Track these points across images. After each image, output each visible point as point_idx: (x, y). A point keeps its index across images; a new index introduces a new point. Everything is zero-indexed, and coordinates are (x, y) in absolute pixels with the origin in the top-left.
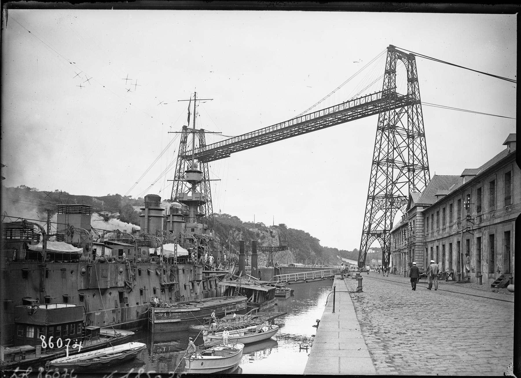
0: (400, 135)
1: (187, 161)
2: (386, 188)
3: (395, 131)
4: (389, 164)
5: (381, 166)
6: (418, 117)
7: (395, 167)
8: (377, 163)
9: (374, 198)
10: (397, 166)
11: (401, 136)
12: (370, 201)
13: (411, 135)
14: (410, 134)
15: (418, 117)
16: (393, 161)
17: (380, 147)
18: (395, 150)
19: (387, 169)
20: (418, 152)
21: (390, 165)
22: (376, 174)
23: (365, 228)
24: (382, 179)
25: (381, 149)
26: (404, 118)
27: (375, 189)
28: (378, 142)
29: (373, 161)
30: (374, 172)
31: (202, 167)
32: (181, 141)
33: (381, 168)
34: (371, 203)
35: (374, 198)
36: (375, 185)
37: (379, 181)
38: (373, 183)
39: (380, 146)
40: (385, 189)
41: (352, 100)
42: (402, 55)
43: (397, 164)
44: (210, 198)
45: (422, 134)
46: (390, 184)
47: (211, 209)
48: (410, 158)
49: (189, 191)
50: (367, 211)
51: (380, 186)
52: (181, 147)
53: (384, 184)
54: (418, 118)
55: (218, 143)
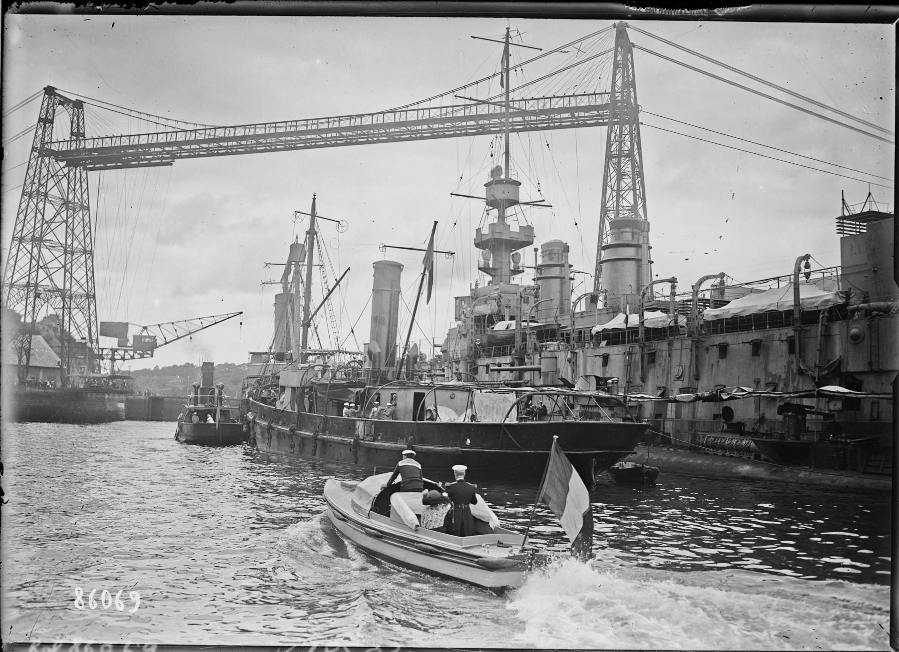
18: (40, 270)
20: (78, 230)
25: (26, 222)
41: (532, 99)
42: (65, 101)
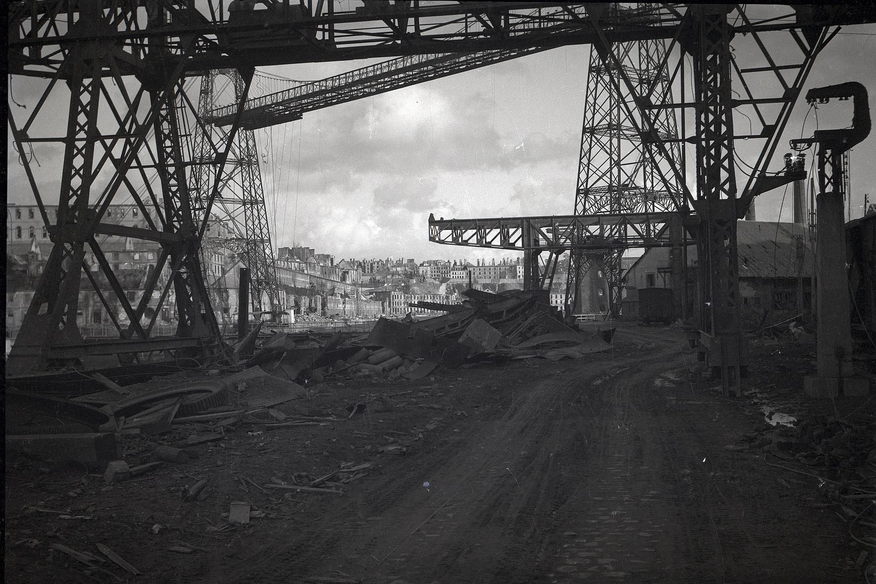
0: (629, 139)
1: (217, 129)
2: (610, 113)
3: (621, 133)
4: (612, 132)
5: (598, 137)
6: (657, 46)
7: (622, 137)
8: (590, 131)
9: (587, 192)
10: (625, 135)
11: (631, 141)
12: (581, 198)
13: (645, 79)
14: (644, 77)
15: (657, 46)
16: (619, 126)
17: (595, 103)
19: (611, 140)
21: (615, 134)
22: (593, 117)
23: (580, 183)
24: (600, 160)
26: (634, 53)
27: (594, 114)
28: (591, 94)
29: (590, 66)
30: (586, 146)
31: (243, 137)
32: (201, 91)
33: (598, 140)
34: (583, 200)
35: (587, 192)
36: (594, 109)
37: (596, 162)
38: (584, 166)
39: (595, 99)
40: (608, 115)
43: (626, 132)
44: (262, 196)
45: (664, 77)
46: (615, 105)
47: (265, 216)
48: (642, 60)
49: (232, 173)
50: (583, 154)
51: (598, 172)
52: (202, 103)
53: (606, 107)
54: (657, 49)
55: (291, 91)
